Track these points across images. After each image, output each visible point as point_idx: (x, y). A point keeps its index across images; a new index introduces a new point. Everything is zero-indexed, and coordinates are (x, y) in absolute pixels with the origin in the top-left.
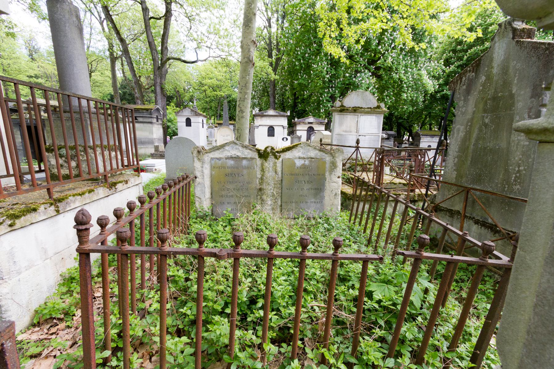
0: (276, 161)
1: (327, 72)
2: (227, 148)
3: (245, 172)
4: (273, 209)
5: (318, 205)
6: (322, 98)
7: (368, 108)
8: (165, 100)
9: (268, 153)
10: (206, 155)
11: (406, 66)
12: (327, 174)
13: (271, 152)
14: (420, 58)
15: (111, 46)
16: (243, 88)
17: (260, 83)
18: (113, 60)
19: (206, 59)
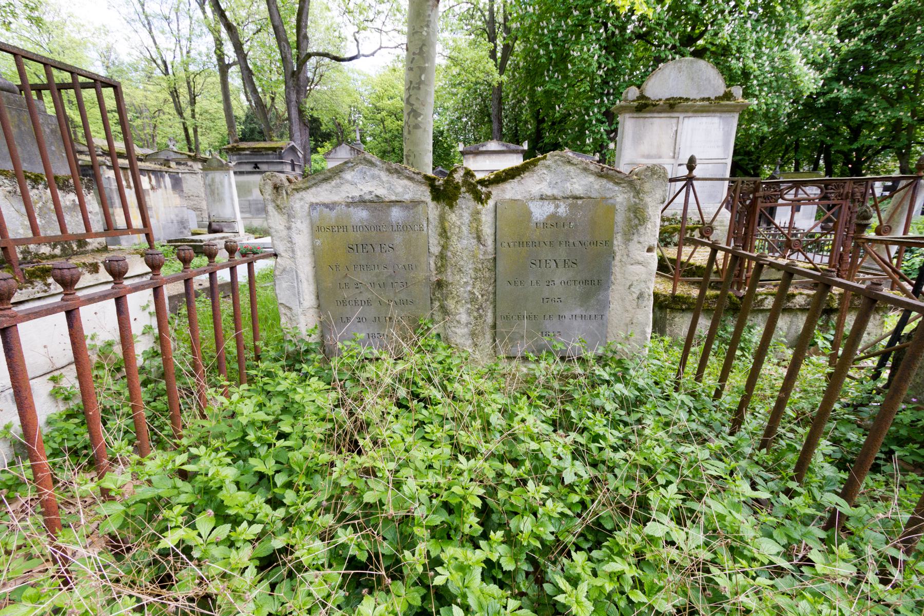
0: (480, 206)
1: (600, 64)
2: (348, 175)
3: (398, 239)
4: (473, 334)
5: (593, 325)
6: (589, 115)
7: (703, 99)
8: (307, 132)
9: (457, 187)
10: (297, 196)
11: (759, 44)
12: (618, 241)
13: (465, 183)
14: (787, 25)
15: (219, 43)
16: (417, 57)
17: (475, 99)
18: (224, 69)
19: (375, 52)
